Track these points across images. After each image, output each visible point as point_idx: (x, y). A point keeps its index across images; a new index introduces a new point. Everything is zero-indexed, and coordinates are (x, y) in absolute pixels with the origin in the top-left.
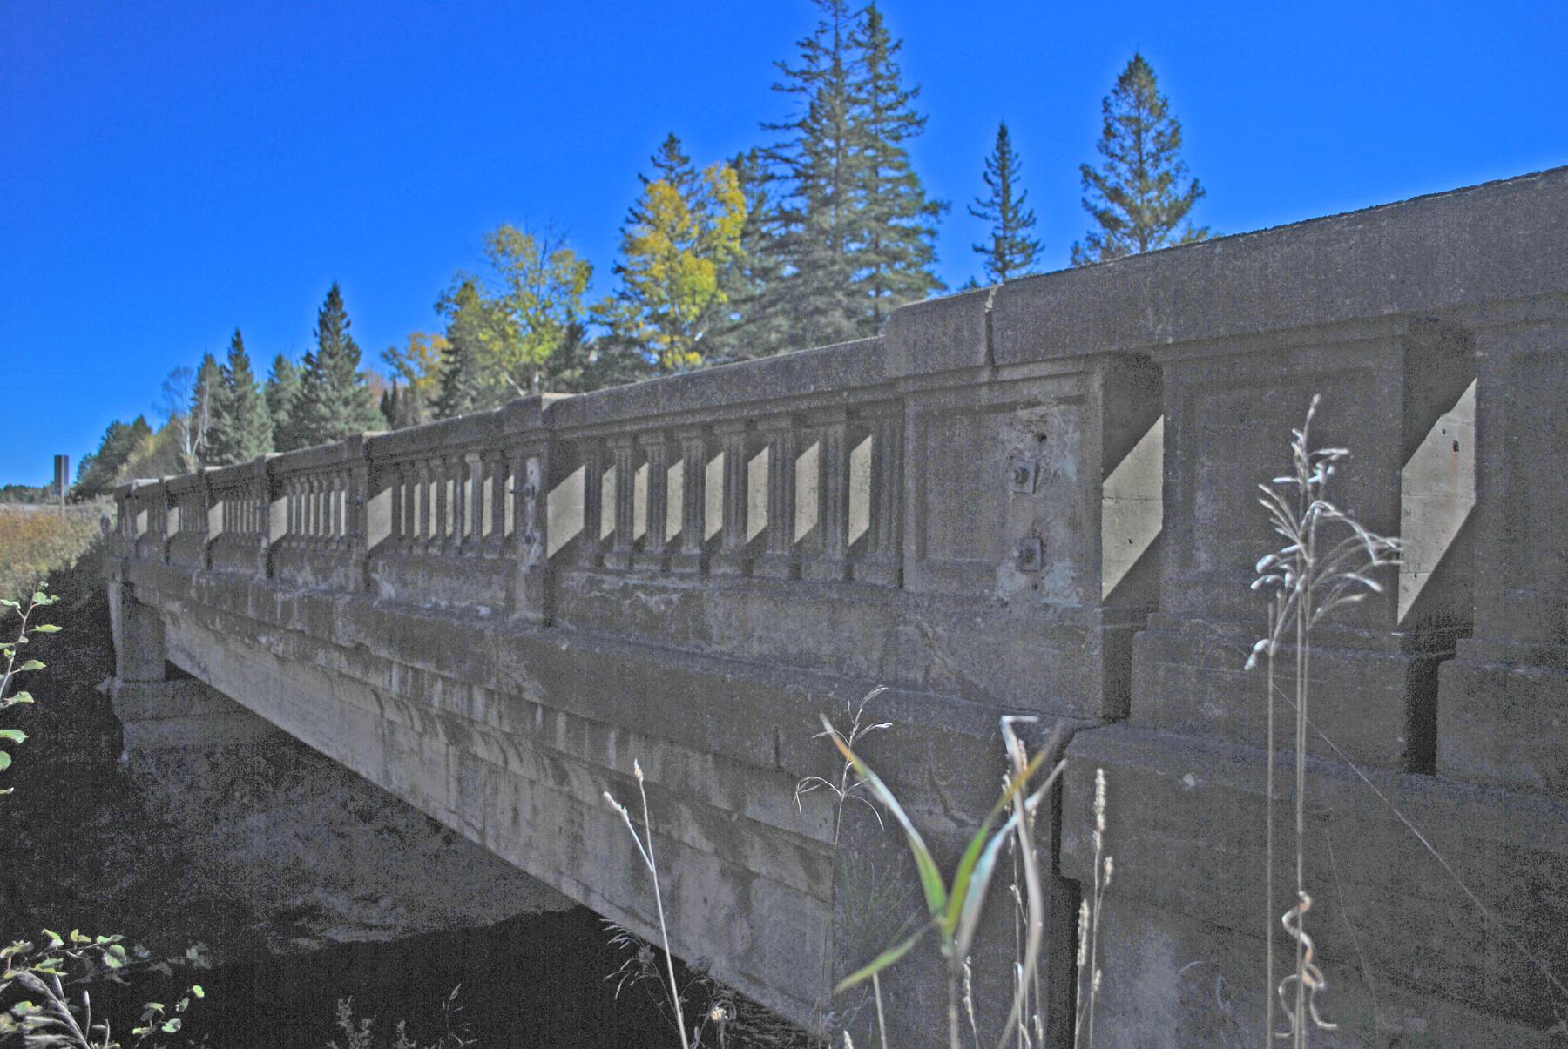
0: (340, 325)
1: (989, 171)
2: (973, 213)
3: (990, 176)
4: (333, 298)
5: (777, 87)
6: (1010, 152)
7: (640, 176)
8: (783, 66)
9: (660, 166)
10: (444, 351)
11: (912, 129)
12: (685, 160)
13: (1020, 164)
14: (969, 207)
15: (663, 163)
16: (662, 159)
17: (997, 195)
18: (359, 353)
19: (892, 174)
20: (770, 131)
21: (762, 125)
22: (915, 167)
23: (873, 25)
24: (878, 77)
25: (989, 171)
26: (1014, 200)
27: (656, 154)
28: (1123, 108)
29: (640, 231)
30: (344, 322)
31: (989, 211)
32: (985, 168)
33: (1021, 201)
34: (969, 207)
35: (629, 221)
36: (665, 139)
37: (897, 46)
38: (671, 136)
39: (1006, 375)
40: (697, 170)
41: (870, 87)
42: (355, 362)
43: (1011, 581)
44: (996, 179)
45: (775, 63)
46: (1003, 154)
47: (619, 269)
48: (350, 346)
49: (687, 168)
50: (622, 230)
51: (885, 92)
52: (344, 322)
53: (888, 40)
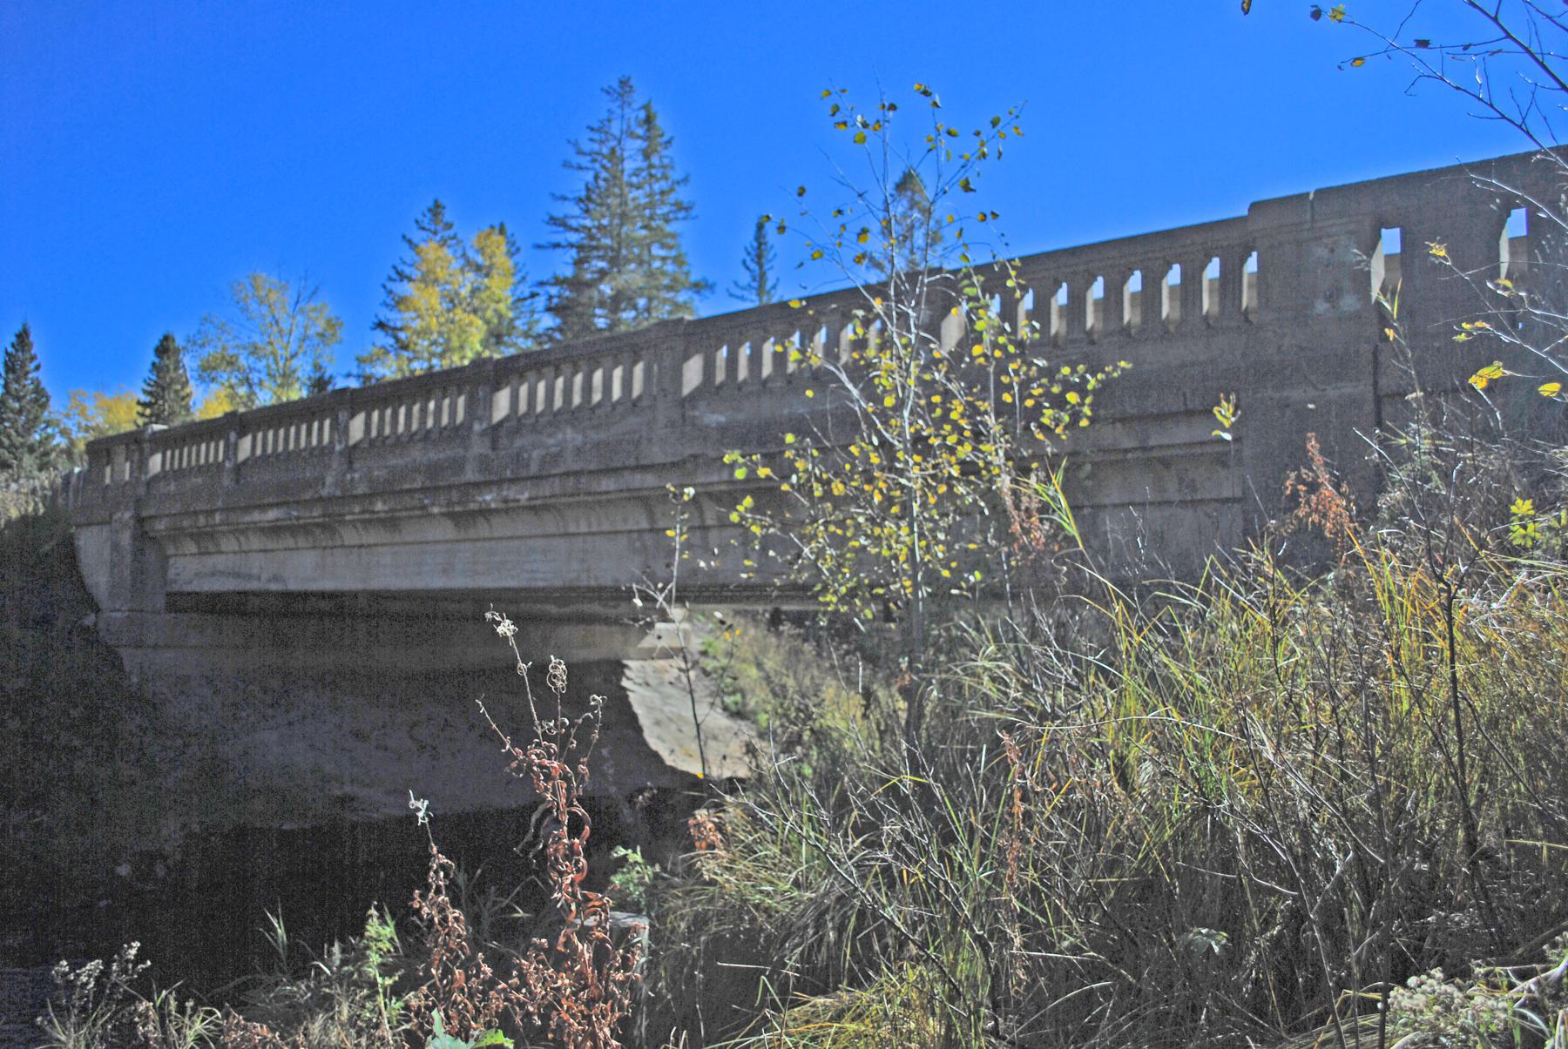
0: (27, 369)
1: (748, 259)
2: (731, 295)
3: (749, 262)
4: (22, 338)
5: (567, 165)
6: (766, 244)
7: (404, 237)
8: (576, 144)
9: (423, 229)
10: (139, 403)
11: (681, 215)
12: (449, 226)
13: (775, 255)
14: (728, 290)
15: (427, 226)
16: (426, 222)
17: (754, 280)
18: (48, 399)
19: (662, 253)
20: (560, 202)
21: (553, 195)
22: (685, 246)
23: (649, 120)
24: (651, 166)
25: (748, 259)
26: (769, 284)
27: (420, 218)
28: (898, 209)
29: (406, 289)
30: (32, 366)
31: (745, 294)
32: (743, 255)
33: (774, 287)
34: (728, 290)
35: (390, 279)
36: (430, 204)
37: (669, 142)
38: (436, 201)
39: (1319, 224)
40: (460, 236)
41: (644, 174)
42: (44, 406)
43: (1321, 307)
44: (753, 266)
45: (569, 142)
46: (760, 244)
47: (381, 325)
48: (39, 390)
49: (451, 233)
50: (384, 287)
51: (658, 180)
52: (32, 366)
53: (661, 136)
